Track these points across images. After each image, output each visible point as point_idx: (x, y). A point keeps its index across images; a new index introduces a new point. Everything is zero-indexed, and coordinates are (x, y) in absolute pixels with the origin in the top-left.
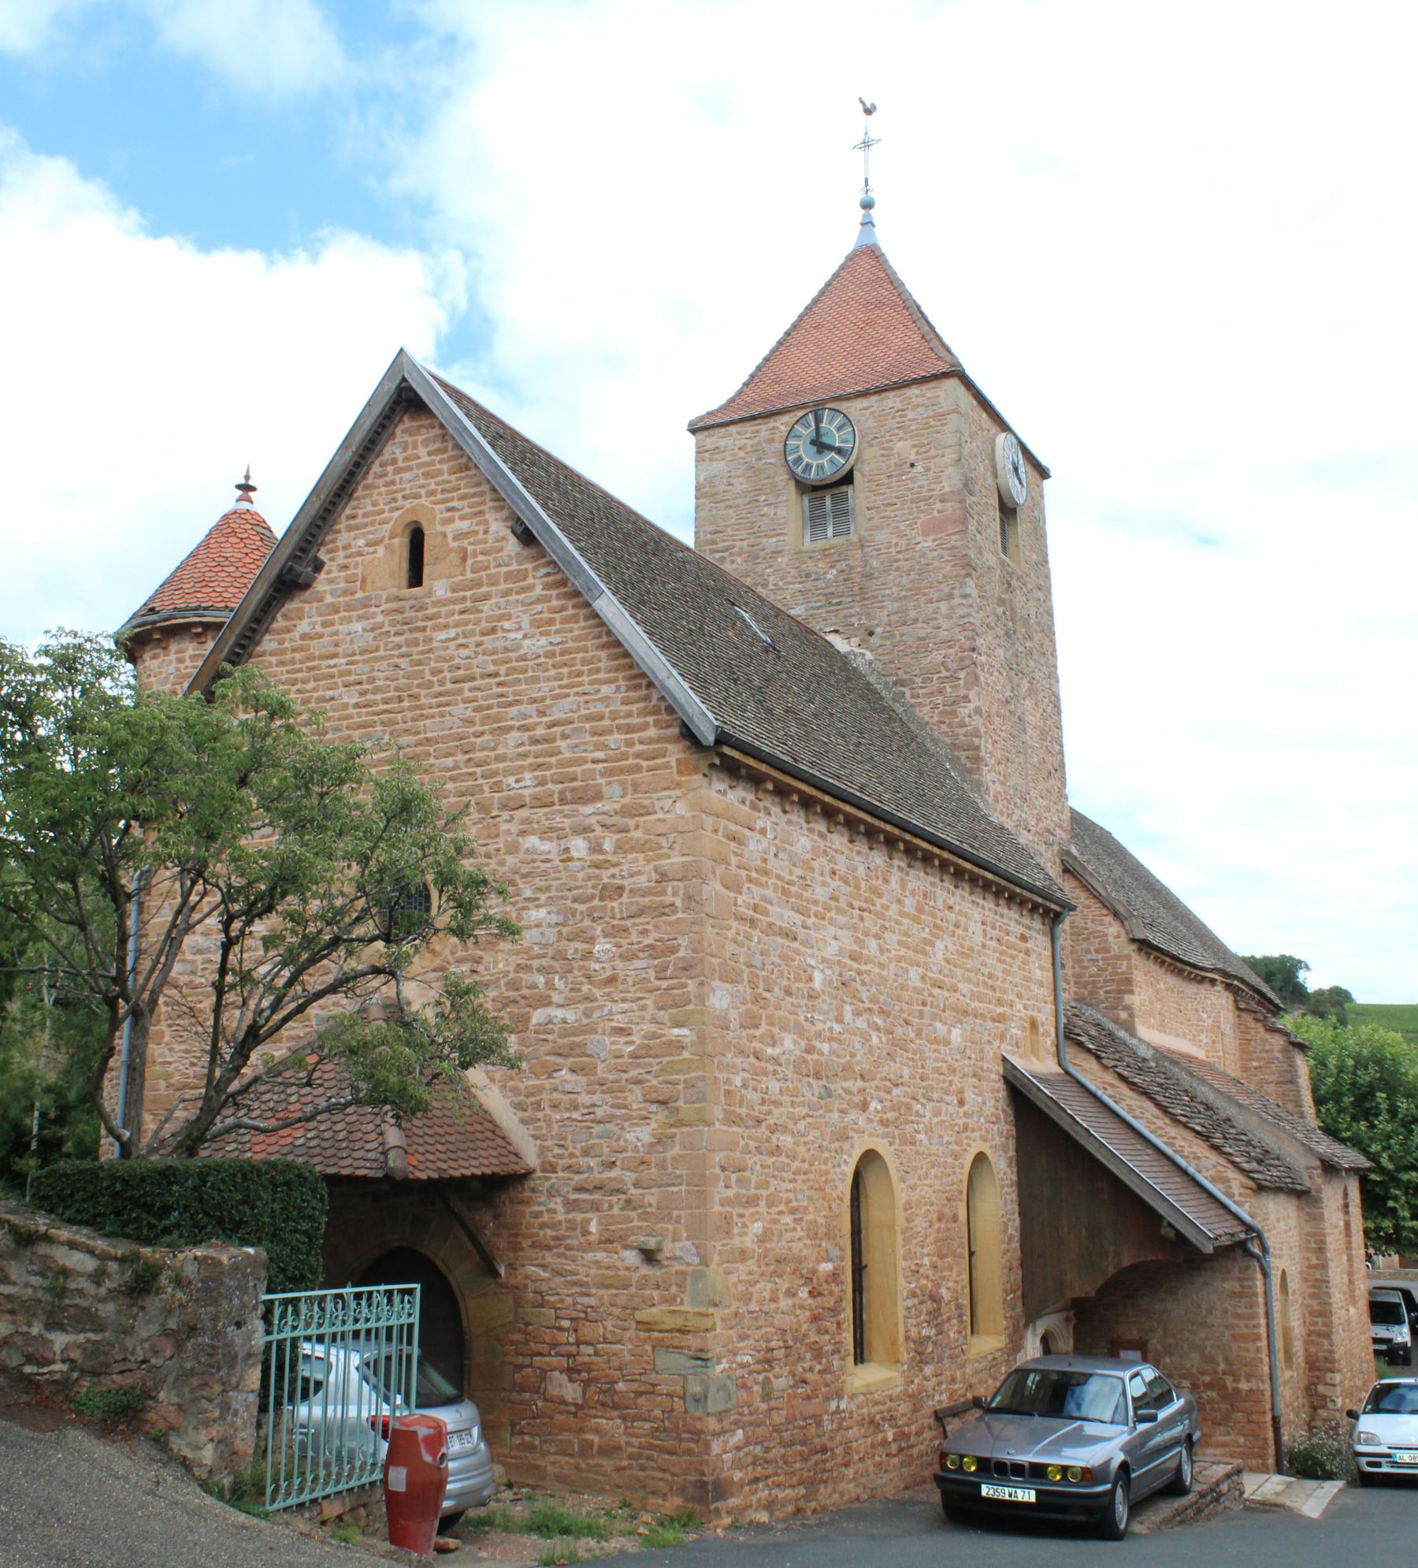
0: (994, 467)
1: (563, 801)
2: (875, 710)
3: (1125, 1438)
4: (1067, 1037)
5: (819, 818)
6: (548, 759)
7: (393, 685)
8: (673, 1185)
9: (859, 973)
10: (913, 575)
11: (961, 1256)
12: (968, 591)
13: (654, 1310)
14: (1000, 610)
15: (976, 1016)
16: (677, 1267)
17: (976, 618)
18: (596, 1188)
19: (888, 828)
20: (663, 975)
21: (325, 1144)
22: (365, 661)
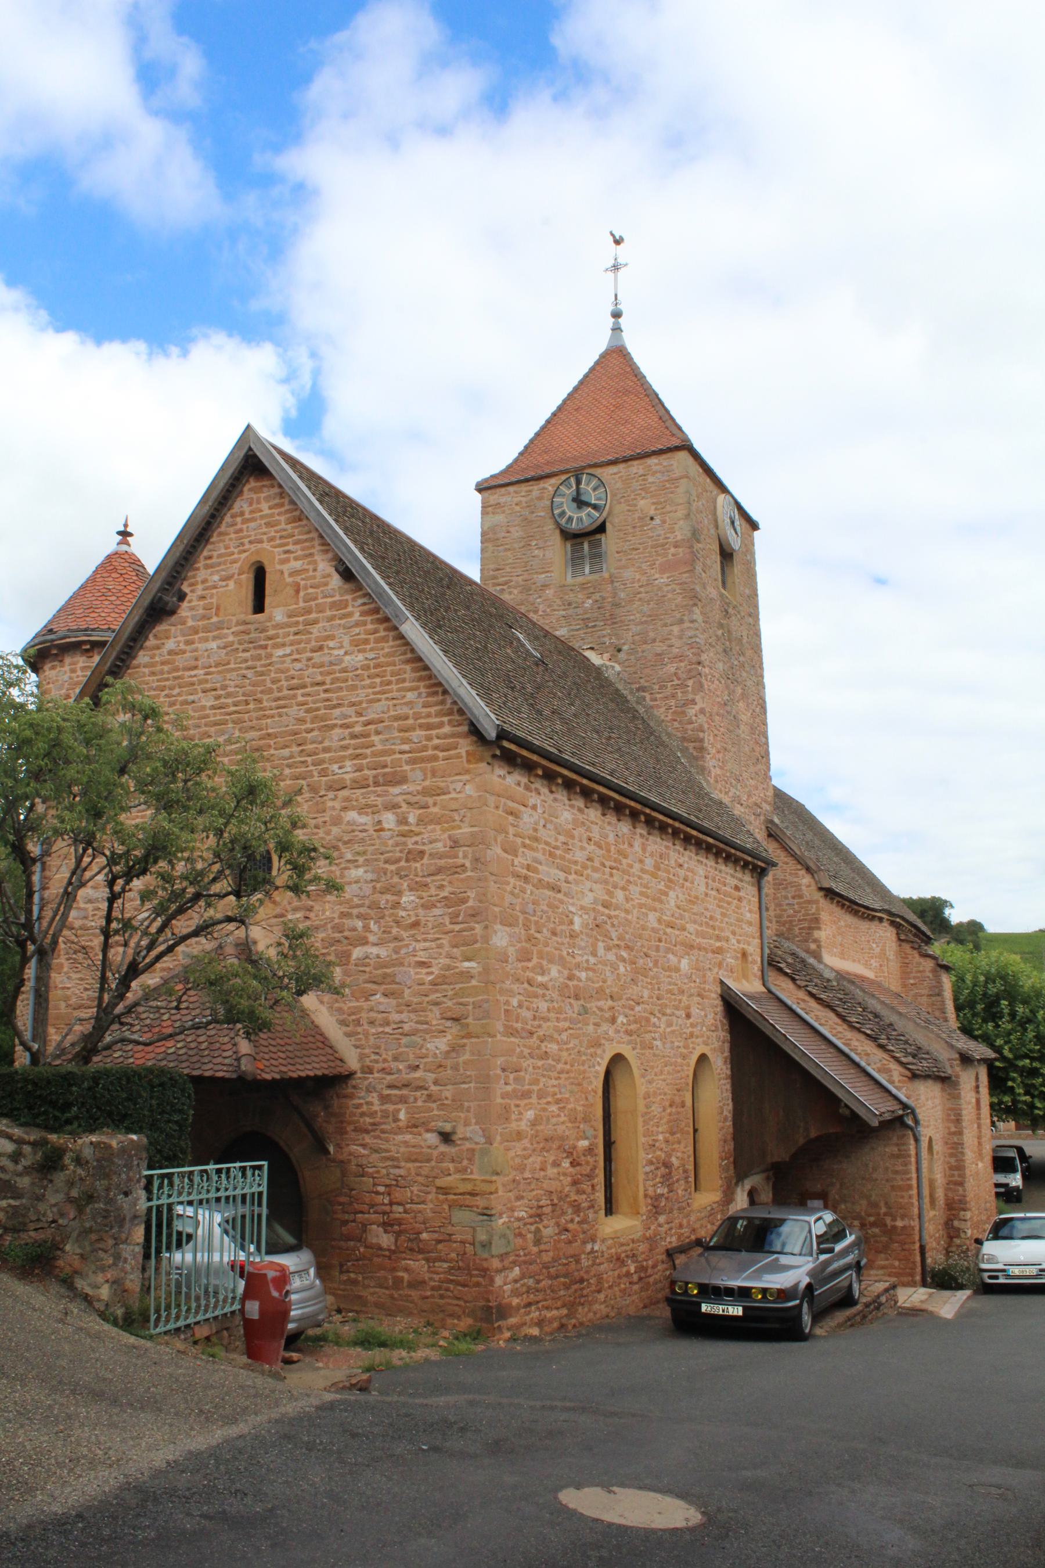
0: (716, 521)
1: (376, 784)
2: (622, 711)
3: (811, 1266)
4: (770, 964)
5: (577, 797)
7: (241, 691)
8: (464, 1083)
9: (610, 917)
10: (652, 605)
12: (695, 617)
13: (449, 1178)
14: (720, 632)
15: (700, 949)
16: (468, 1145)
17: (701, 639)
21: (191, 1053)
22: (219, 672)
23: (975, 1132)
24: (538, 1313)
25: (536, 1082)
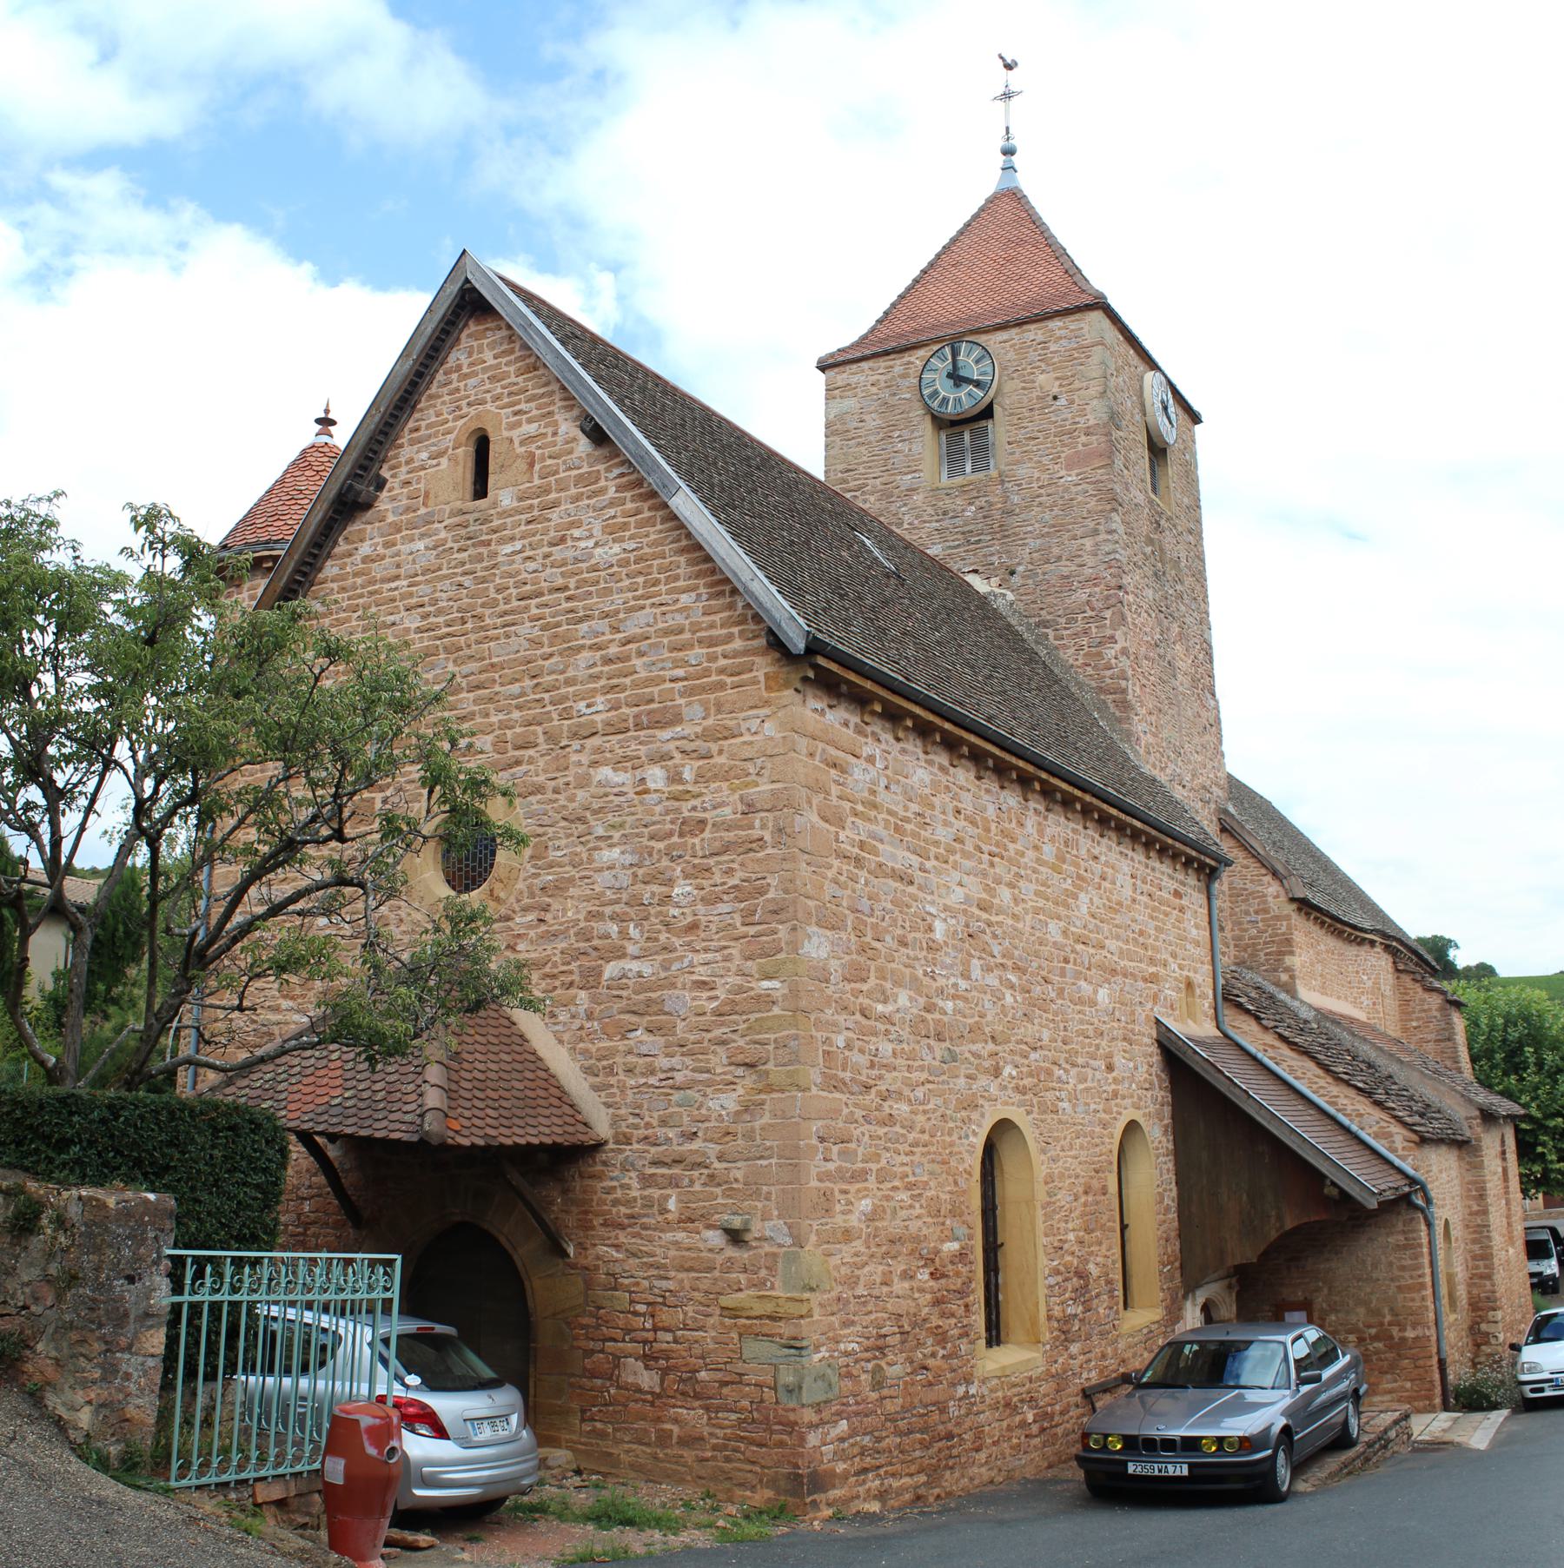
0: (1143, 405)
1: (639, 726)
2: (1014, 650)
3: (1288, 1401)
4: (1225, 999)
5: (938, 749)
6: (623, 680)
7: (456, 605)
8: (761, 1158)
10: (1056, 511)
11: (1112, 1230)
12: (1114, 526)
14: (1148, 550)
15: (1125, 976)
16: (767, 1248)
17: (1123, 555)
18: (675, 1161)
19: (1021, 764)
20: (748, 920)
21: (361, 1105)
22: (428, 582)
24: (877, 1482)
25: (876, 1157)
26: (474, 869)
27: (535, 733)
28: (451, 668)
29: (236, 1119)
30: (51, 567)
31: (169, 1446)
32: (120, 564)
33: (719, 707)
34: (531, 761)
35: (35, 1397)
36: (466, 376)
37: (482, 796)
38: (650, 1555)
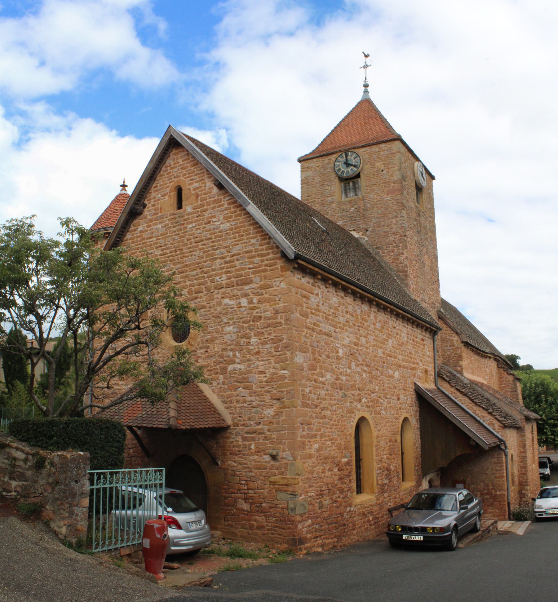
1: (238, 285)
3: (456, 515)
4: (438, 376)
5: (341, 291)
8: (282, 430)
9: (358, 350)
10: (383, 209)
11: (398, 454)
12: (403, 215)
13: (276, 477)
14: (415, 223)
15: (404, 368)
16: (284, 461)
17: (406, 225)
19: (369, 295)
20: (277, 350)
21: (149, 416)
22: (163, 238)
23: (532, 452)
24: (321, 541)
25: (320, 430)
26: (183, 335)
27: (202, 288)
28: (172, 266)
29: (108, 425)
30: (33, 241)
31: (92, 538)
32: (56, 238)
33: (265, 278)
34: (201, 297)
35: (47, 524)
36: (173, 168)
37: (186, 311)
38: (248, 568)
